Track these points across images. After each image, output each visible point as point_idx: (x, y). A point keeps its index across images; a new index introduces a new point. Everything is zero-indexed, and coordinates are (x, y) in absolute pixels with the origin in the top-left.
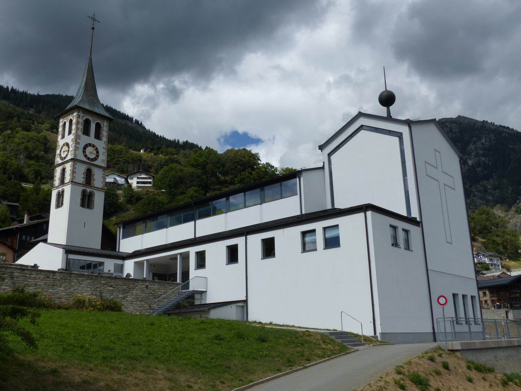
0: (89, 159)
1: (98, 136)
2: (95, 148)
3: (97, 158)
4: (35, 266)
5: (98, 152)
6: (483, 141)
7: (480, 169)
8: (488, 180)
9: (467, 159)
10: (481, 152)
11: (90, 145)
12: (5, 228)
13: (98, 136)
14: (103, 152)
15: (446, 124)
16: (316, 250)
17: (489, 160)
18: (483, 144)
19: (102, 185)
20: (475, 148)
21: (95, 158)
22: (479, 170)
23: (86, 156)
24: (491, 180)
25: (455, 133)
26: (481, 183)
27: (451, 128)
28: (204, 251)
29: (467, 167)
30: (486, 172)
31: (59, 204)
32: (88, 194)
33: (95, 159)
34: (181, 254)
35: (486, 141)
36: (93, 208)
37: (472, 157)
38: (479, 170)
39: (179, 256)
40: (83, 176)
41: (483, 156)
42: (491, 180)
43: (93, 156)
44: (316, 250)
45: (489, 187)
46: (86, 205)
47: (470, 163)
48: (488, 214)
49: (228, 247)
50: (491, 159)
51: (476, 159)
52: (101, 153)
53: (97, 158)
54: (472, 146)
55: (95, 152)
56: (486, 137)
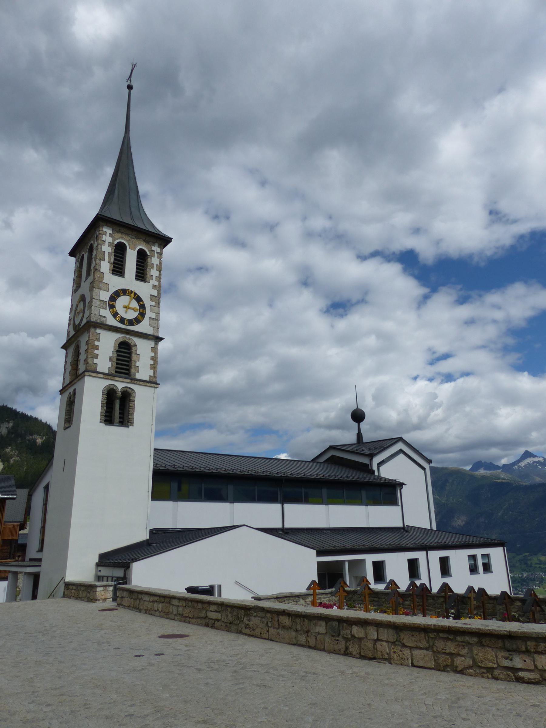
0: (122, 321)
2: (132, 295)
3: (140, 318)
5: (142, 307)
11: (124, 292)
12: (256, 494)
16: (155, 449)
21: (136, 319)
23: (115, 315)
28: (39, 572)
32: (119, 394)
33: (137, 321)
34: (349, 561)
36: (132, 424)
39: (347, 564)
40: (138, 364)
43: (132, 315)
44: (155, 449)
46: (117, 419)
49: (441, 559)
53: (140, 318)
55: (135, 304)
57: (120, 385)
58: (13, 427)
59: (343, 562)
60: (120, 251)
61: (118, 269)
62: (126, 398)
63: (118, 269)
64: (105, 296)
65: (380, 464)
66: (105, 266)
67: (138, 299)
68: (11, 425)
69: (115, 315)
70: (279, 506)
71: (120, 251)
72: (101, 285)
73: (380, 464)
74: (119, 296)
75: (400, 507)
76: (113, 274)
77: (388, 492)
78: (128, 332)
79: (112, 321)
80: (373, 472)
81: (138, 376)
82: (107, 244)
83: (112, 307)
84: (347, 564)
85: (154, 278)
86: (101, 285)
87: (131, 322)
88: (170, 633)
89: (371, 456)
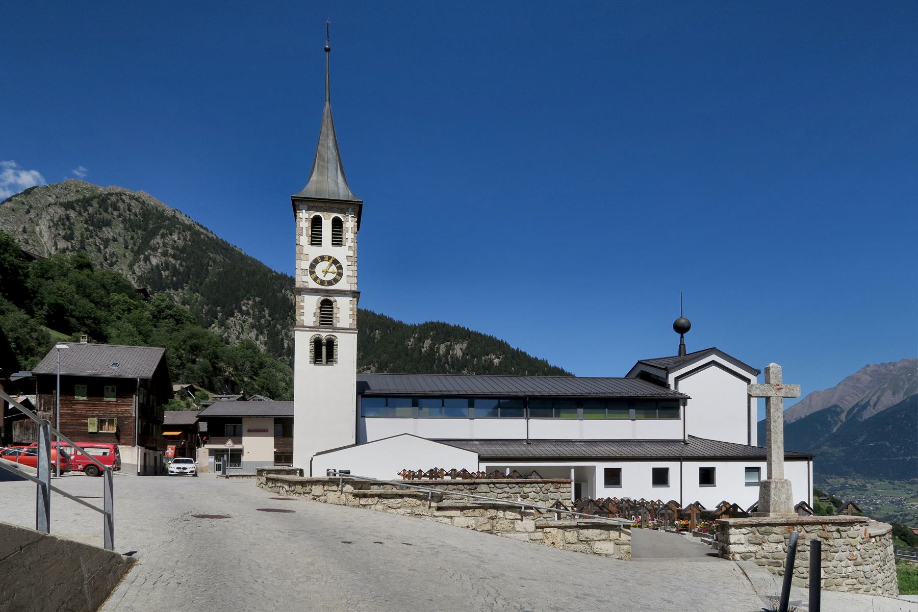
0: (322, 283)
1: (337, 240)
3: (338, 278)
4: (464, 471)
5: (340, 267)
6: (175, 237)
7: (167, 273)
8: (176, 290)
9: (150, 254)
10: (170, 251)
11: (322, 258)
13: (337, 240)
14: (350, 271)
15: (123, 197)
17: (181, 265)
18: (175, 242)
19: (314, 319)
20: (164, 243)
22: (165, 274)
23: (316, 279)
24: (180, 290)
25: (136, 215)
26: (167, 291)
27: (129, 205)
29: (149, 266)
30: (175, 279)
31: (324, 351)
32: (324, 341)
33: (336, 281)
34: (575, 467)
35: (179, 239)
37: (158, 254)
38: (165, 274)
39: (573, 470)
41: (174, 257)
42: (180, 290)
43: (330, 277)
45: (176, 299)
47: (154, 261)
48: (255, 353)
50: (184, 263)
51: (163, 259)
52: (345, 273)
53: (338, 278)
54: (158, 240)
55: (334, 268)
56: (179, 233)
57: (324, 335)
58: (467, 348)
59: (570, 468)
60: (316, 223)
61: (316, 240)
62: (331, 344)
63: (316, 240)
64: (306, 265)
65: (677, 379)
66: (304, 240)
67: (335, 262)
68: (465, 345)
69: (316, 279)
70: (524, 421)
71: (316, 223)
72: (302, 256)
73: (677, 379)
74: (318, 263)
75: (681, 422)
76: (312, 244)
77: (212, 452)
78: (327, 291)
79: (313, 285)
80: (668, 387)
81: (339, 325)
82: (304, 220)
83: (312, 273)
84: (573, 470)
85: (349, 240)
86: (302, 256)
87: (330, 283)
88: (215, 521)
89: (667, 371)
